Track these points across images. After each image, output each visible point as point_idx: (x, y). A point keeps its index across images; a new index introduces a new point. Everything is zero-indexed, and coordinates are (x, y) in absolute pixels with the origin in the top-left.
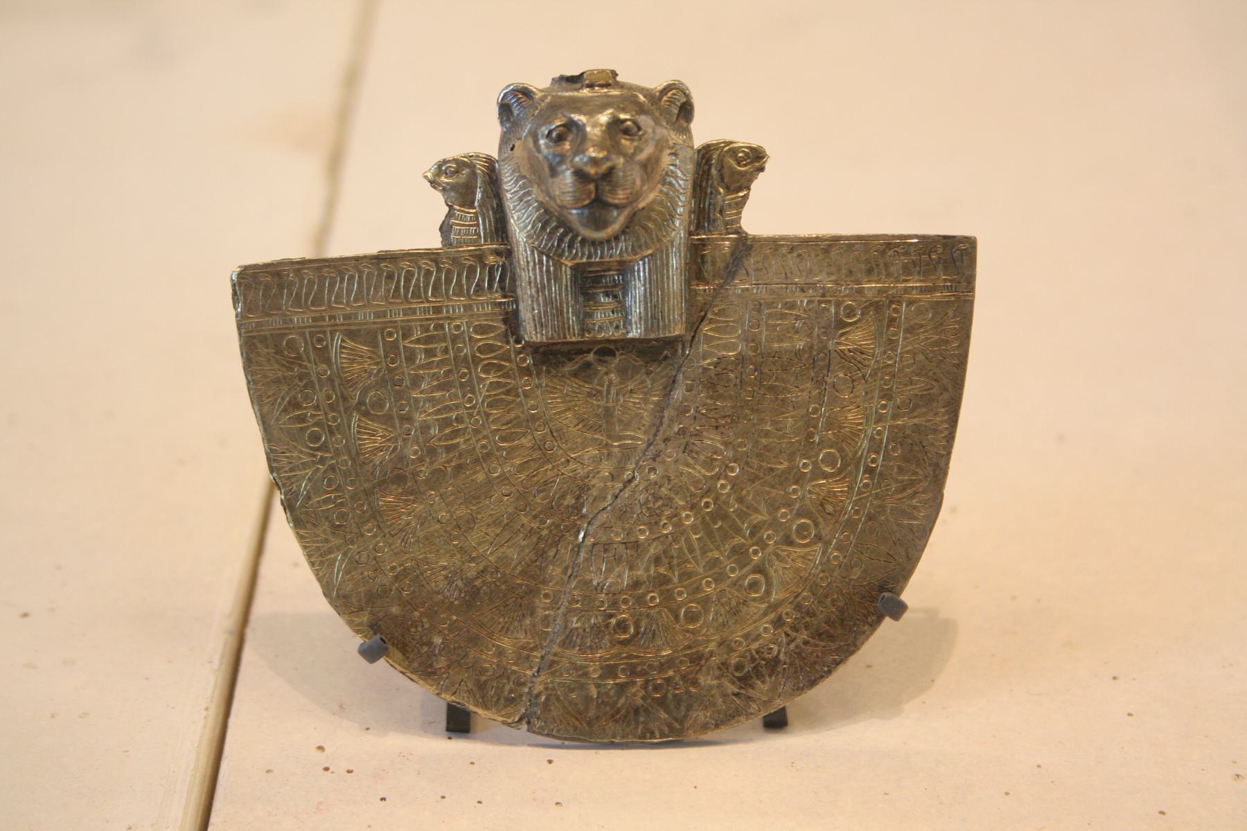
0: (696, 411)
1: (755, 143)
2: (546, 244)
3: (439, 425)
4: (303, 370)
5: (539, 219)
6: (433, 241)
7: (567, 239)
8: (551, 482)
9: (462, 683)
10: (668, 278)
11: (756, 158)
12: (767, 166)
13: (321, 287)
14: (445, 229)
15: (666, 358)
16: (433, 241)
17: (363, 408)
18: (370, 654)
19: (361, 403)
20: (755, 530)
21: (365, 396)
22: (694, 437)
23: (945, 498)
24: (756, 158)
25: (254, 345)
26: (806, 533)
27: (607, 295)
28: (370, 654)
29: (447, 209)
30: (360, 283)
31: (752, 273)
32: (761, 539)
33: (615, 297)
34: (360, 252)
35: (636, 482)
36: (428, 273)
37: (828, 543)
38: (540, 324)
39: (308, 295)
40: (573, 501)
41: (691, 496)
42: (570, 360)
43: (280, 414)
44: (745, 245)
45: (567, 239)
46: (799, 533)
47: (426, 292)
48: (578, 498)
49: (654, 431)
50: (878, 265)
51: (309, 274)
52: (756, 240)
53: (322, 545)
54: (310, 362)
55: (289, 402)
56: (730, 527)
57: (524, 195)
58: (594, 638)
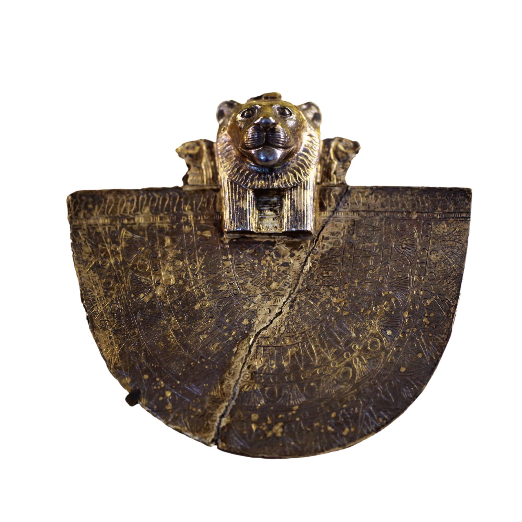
1: (353, 139)
3: (217, 319)
4: (103, 247)
6: (180, 184)
7: (250, 177)
8: (236, 311)
10: (304, 199)
11: (355, 147)
12: (360, 151)
14: (185, 178)
15: (302, 248)
16: (180, 184)
17: (135, 268)
18: (132, 400)
19: (134, 265)
20: (347, 343)
21: (136, 261)
23: (169, 432)
24: (355, 147)
25: (103, 252)
26: (376, 346)
27: (271, 210)
28: (132, 400)
29: (187, 169)
30: (137, 203)
31: (350, 204)
32: (350, 348)
33: (275, 211)
34: (140, 188)
35: (283, 313)
36: (175, 199)
37: (387, 352)
38: (233, 220)
39: (109, 207)
42: (249, 247)
43: (89, 271)
44: (347, 190)
45: (250, 177)
46: (372, 346)
48: (250, 321)
51: (110, 197)
52: (354, 188)
54: (107, 243)
55: (95, 264)
56: (334, 340)
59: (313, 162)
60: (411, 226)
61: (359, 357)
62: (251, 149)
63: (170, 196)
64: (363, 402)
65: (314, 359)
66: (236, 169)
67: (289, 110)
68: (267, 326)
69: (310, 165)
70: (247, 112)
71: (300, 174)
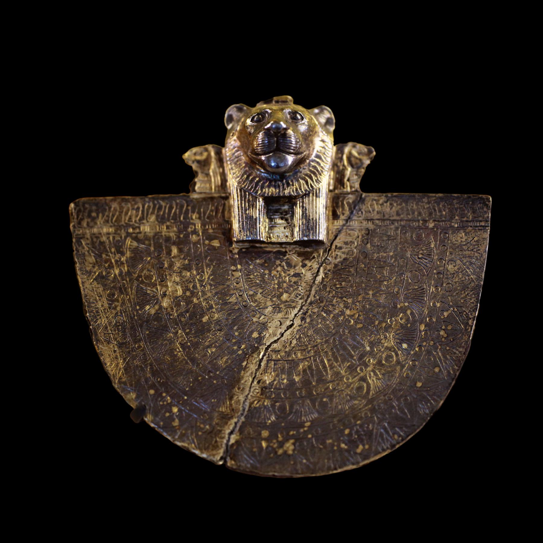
2: (248, 187)
4: (107, 257)
5: (245, 173)
7: (260, 184)
8: (245, 324)
9: (358, 270)
10: (316, 207)
15: (314, 257)
17: (140, 279)
20: (361, 357)
30: (143, 211)
31: (364, 213)
32: (365, 361)
33: (286, 220)
35: (295, 326)
36: (182, 207)
37: (403, 366)
38: (242, 229)
42: (259, 257)
43: (93, 281)
46: (387, 360)
48: (260, 334)
49: (337, 240)
53: (348, 347)
55: (98, 275)
56: (347, 354)
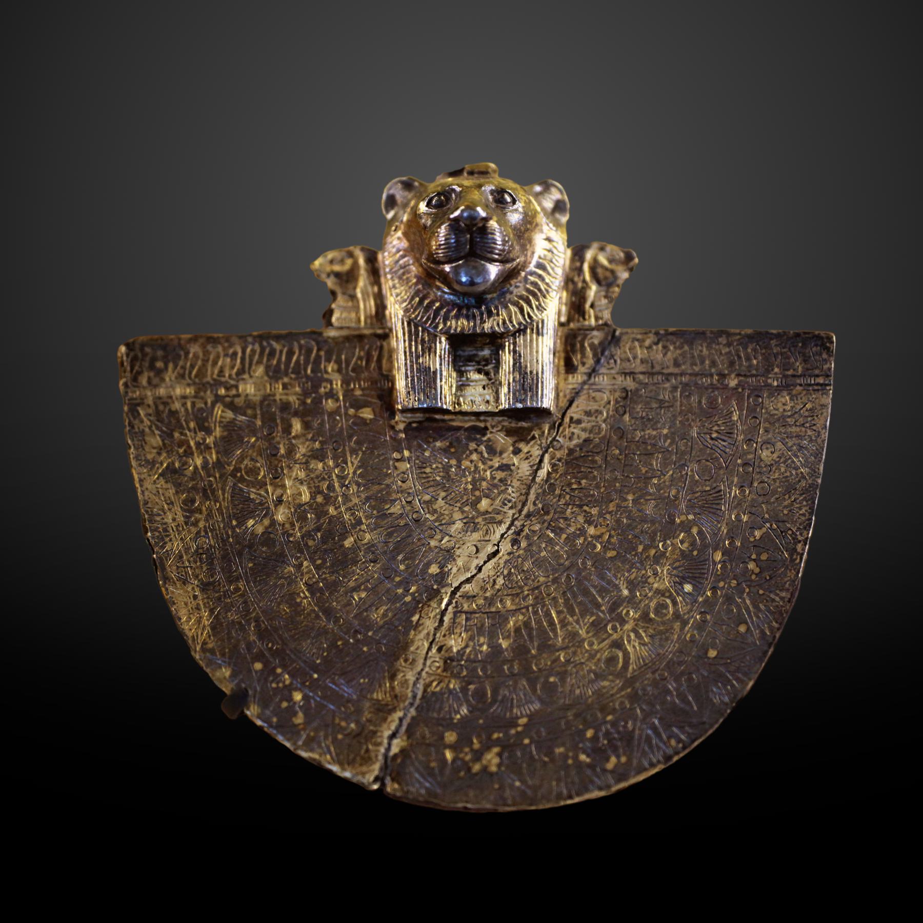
0: (561, 490)
2: (422, 317)
4: (183, 437)
7: (442, 313)
8: (417, 551)
10: (537, 352)
13: (205, 361)
15: (534, 438)
17: (239, 475)
19: (238, 469)
20: (614, 607)
22: (570, 435)
25: (183, 446)
26: (664, 611)
30: (243, 359)
31: (619, 361)
32: (620, 614)
33: (487, 374)
35: (501, 554)
36: (309, 351)
37: (685, 623)
38: (411, 389)
40: (438, 571)
41: (552, 570)
42: (441, 436)
43: (158, 478)
45: (442, 313)
46: (658, 612)
47: (306, 370)
50: (739, 357)
56: (590, 602)
57: (404, 274)
58: (256, 578)
59: (554, 287)
60: (727, 400)
61: (634, 630)
62: (444, 263)
63: (301, 347)
64: (642, 710)
65: (556, 635)
66: (417, 299)
67: (511, 195)
68: (473, 577)
69: (547, 291)
70: (436, 198)
71: (531, 307)
